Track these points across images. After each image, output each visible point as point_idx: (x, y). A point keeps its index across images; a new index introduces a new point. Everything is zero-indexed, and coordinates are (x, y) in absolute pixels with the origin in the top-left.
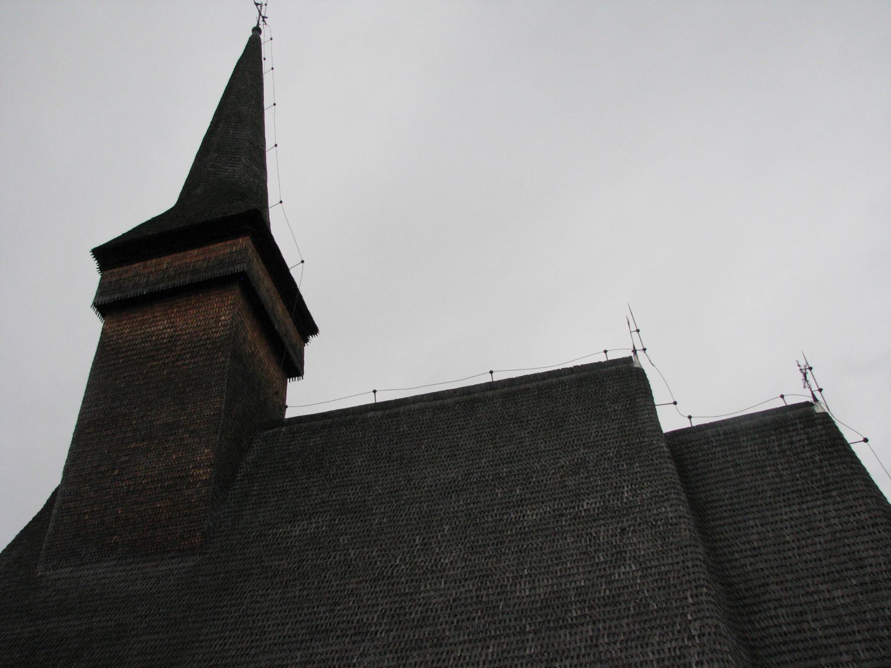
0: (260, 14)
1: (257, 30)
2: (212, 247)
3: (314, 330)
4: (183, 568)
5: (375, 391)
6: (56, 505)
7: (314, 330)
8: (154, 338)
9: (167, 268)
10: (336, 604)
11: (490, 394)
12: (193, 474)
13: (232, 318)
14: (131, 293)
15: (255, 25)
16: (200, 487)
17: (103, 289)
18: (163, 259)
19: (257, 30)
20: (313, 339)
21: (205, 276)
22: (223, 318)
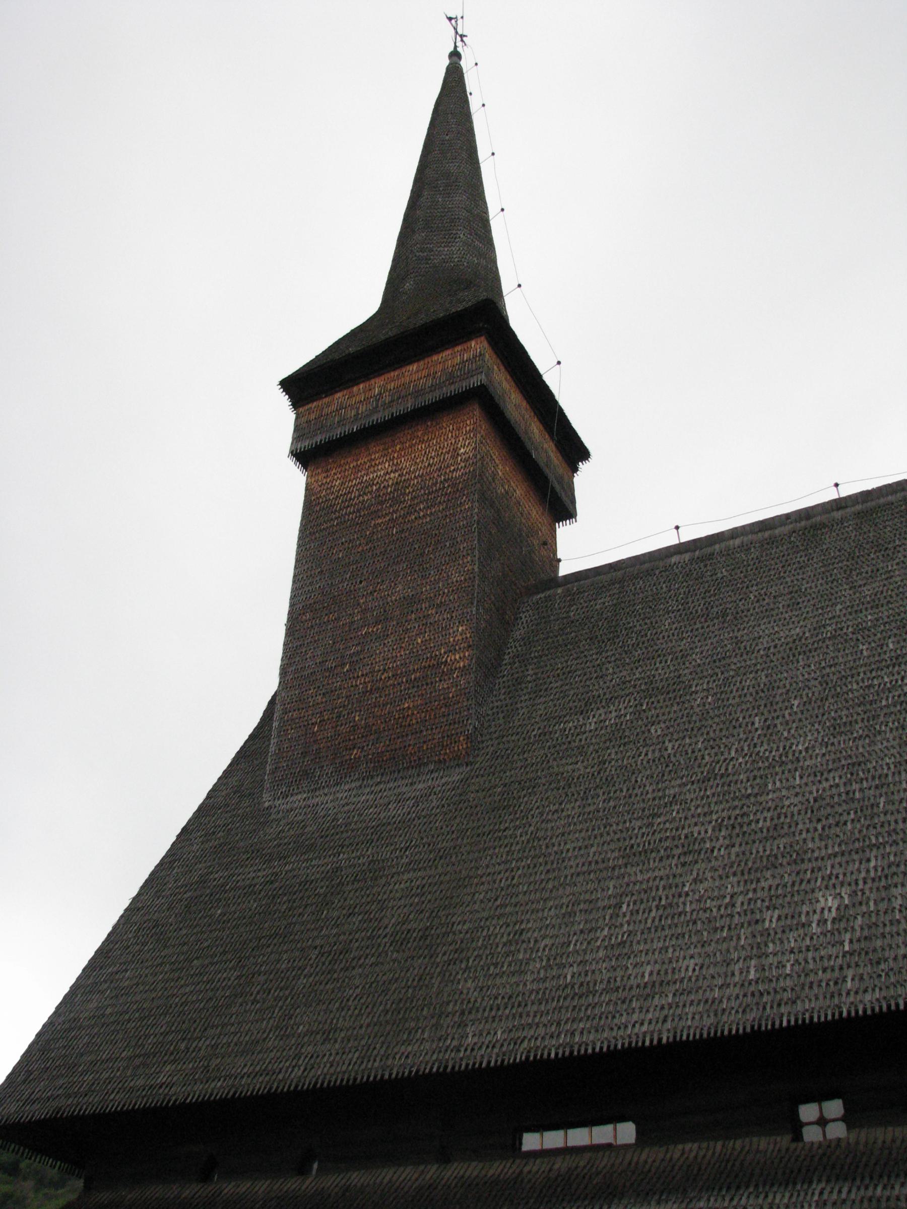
0: (457, 33)
1: (455, 55)
2: (435, 358)
3: (582, 453)
4: (446, 783)
5: (677, 528)
6: (276, 715)
7: (582, 453)
8: (374, 488)
9: (380, 394)
10: (655, 815)
11: (838, 515)
12: (446, 661)
13: (475, 448)
14: (338, 432)
15: (452, 49)
16: (457, 677)
17: (299, 432)
18: (373, 381)
19: (455, 55)
20: (583, 467)
21: (430, 398)
22: (462, 450)
